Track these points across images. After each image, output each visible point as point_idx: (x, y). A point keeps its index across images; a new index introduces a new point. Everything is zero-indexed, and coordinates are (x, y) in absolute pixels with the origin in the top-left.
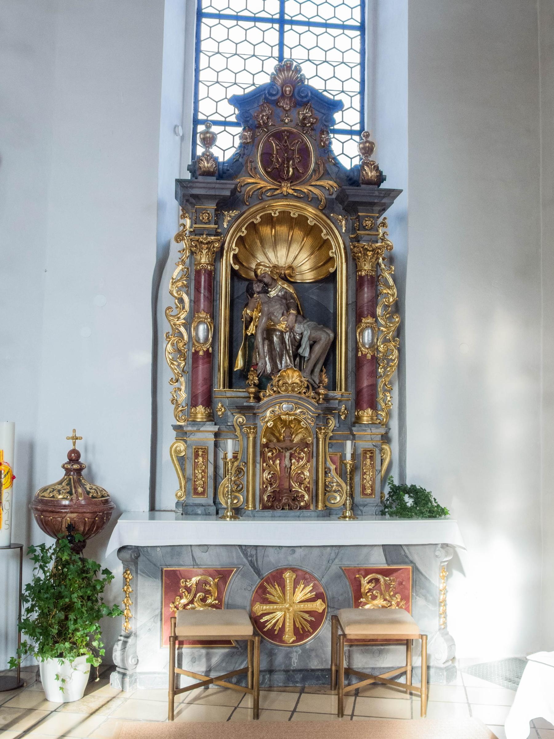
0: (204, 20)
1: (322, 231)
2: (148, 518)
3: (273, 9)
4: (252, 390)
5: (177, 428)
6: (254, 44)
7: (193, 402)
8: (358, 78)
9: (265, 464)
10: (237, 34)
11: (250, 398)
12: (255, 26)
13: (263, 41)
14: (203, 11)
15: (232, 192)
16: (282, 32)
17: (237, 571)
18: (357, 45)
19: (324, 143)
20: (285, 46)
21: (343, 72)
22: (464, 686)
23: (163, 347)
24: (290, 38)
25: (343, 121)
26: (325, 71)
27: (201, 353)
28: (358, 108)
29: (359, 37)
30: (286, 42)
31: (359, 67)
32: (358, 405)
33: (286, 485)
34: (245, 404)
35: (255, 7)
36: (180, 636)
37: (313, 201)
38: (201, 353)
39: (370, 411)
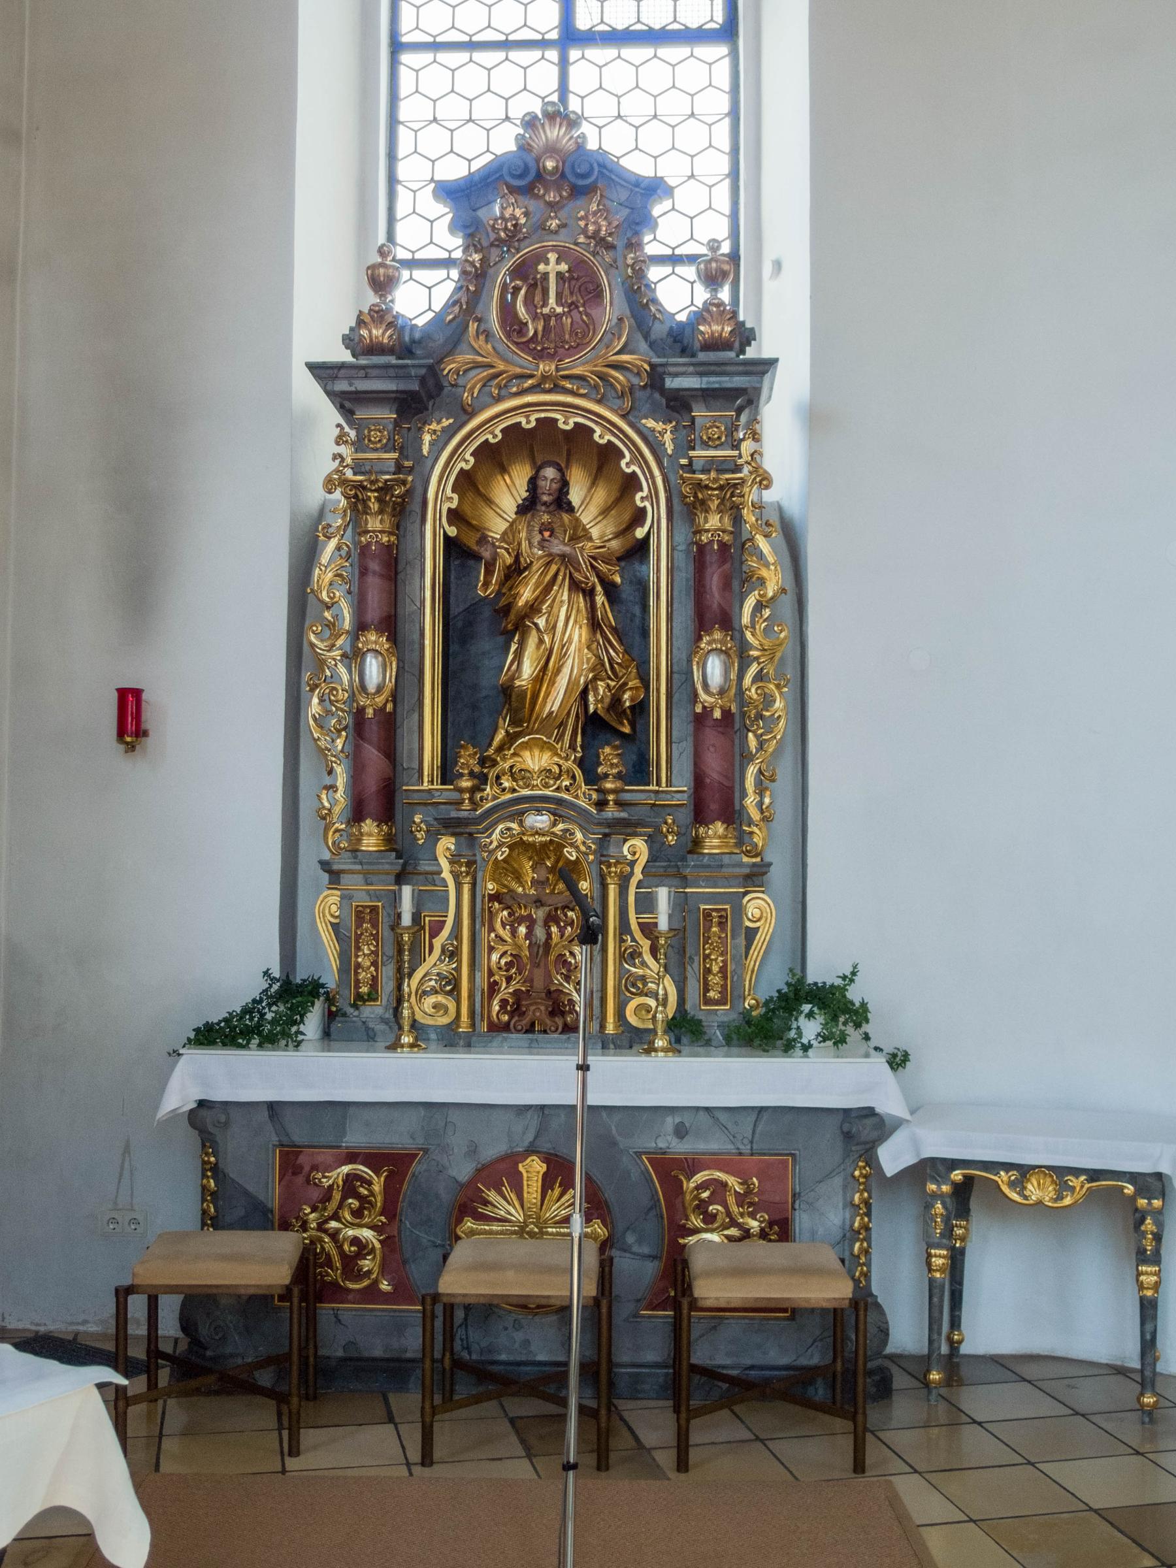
0: (405, 58)
1: (624, 456)
2: (976, 1181)
3: (546, 19)
4: (466, 783)
5: (325, 865)
6: (510, 101)
7: (357, 814)
8: (726, 146)
9: (493, 935)
10: (471, 78)
11: (461, 802)
12: (507, 59)
13: (418, 8)
14: (404, 39)
15: (423, 381)
16: (564, 64)
17: (423, 1155)
18: (722, 74)
19: (633, 269)
20: (571, 95)
21: (692, 136)
22: (396, 1425)
23: (411, 751)
24: (581, 75)
25: (417, 28)
26: (655, 137)
27: (370, 712)
28: (727, 210)
29: (727, 61)
30: (573, 85)
31: (727, 121)
32: (700, 815)
33: (539, 984)
34: (454, 814)
35: (507, 20)
36: (443, 1294)
37: (601, 388)
38: (370, 712)
39: (719, 827)
